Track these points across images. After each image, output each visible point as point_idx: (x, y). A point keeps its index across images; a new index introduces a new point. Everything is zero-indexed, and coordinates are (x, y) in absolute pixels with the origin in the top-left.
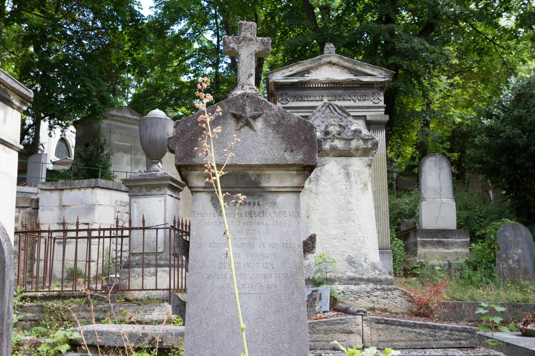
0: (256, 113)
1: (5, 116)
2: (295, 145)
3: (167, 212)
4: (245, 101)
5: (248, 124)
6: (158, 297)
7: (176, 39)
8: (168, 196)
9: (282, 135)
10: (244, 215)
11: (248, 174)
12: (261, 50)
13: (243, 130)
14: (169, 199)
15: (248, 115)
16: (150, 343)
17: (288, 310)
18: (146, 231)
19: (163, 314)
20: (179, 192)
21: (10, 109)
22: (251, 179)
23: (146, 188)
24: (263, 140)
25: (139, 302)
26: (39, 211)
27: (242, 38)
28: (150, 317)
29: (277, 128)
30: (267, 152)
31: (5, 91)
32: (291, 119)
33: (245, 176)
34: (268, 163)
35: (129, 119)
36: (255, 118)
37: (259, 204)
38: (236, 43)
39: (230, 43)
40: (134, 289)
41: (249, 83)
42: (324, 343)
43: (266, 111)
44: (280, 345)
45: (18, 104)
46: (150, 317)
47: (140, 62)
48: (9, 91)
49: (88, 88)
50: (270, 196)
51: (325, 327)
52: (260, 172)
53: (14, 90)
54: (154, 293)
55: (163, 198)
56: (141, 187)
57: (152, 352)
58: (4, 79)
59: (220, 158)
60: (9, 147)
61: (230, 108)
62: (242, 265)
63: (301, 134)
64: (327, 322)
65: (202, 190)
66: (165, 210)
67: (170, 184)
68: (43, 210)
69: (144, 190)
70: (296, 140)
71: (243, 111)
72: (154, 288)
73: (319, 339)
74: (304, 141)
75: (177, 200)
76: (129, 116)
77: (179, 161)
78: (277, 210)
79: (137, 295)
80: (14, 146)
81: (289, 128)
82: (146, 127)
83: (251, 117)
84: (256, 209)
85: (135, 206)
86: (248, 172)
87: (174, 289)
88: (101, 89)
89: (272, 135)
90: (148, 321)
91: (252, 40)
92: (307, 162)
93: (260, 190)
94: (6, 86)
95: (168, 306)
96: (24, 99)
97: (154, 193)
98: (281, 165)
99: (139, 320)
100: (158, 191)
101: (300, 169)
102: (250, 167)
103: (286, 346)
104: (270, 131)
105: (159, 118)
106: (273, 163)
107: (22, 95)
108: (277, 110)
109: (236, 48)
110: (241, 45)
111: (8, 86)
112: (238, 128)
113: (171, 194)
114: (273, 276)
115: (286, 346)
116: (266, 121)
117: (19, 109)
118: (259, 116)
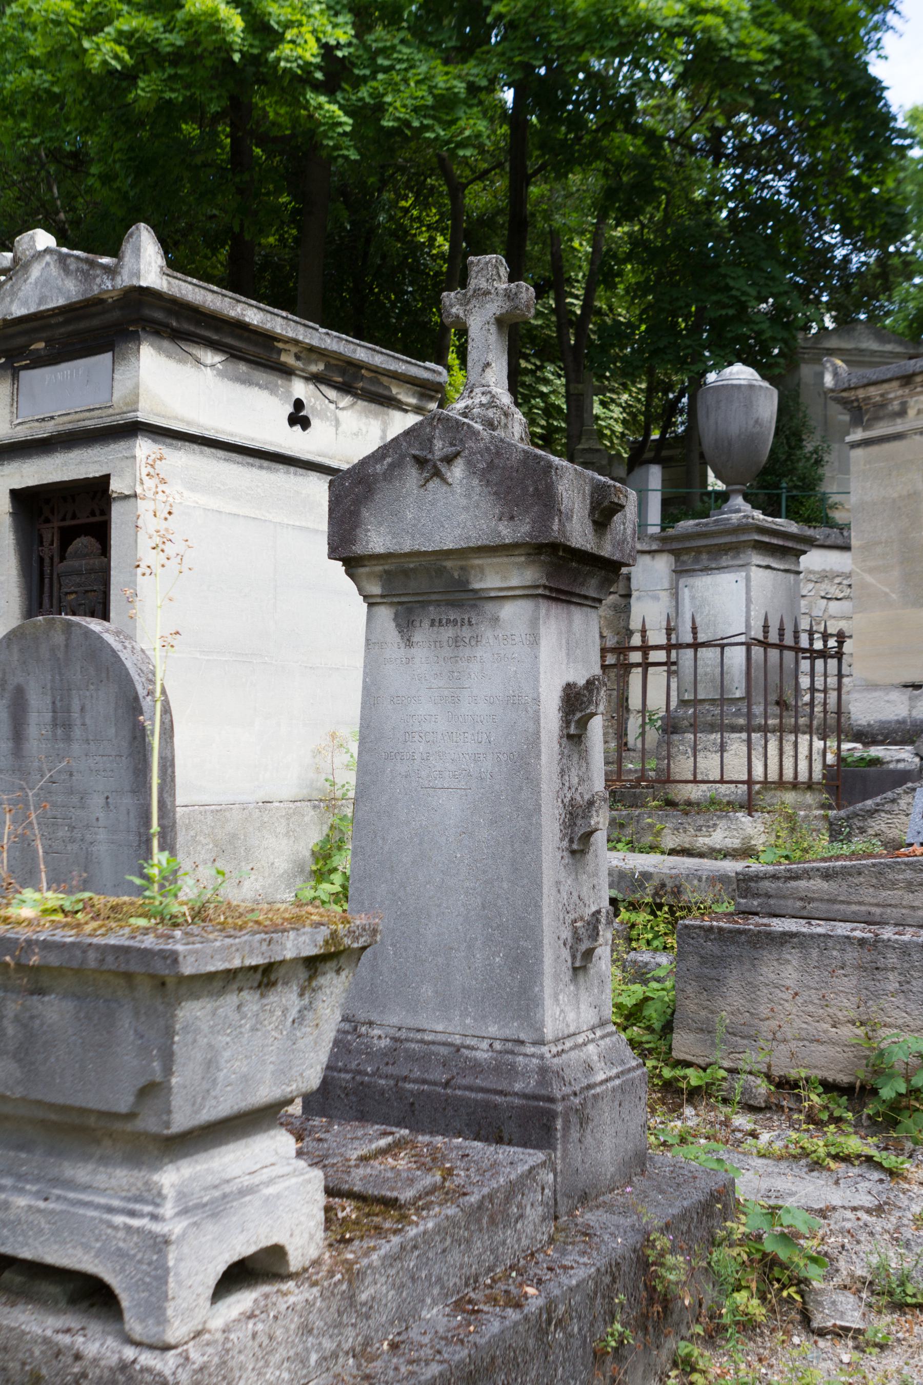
0: (450, 449)
2: (517, 506)
3: (752, 607)
4: (434, 428)
5: (437, 473)
6: (733, 797)
8: (754, 568)
10: (445, 644)
12: (504, 311)
13: (431, 485)
14: (758, 575)
15: (438, 454)
16: (656, 894)
17: (510, 820)
18: (702, 652)
19: (734, 837)
20: (798, 557)
22: (452, 576)
23: (709, 553)
24: (464, 502)
25: (690, 807)
26: (633, 601)
27: (471, 293)
28: (707, 840)
32: (511, 455)
33: (441, 571)
34: (471, 545)
35: (873, 353)
36: (449, 460)
37: (469, 622)
38: (461, 305)
39: (451, 306)
40: (684, 778)
42: (904, 911)
43: (470, 444)
44: (496, 883)
45: (413, 401)
46: (707, 840)
48: (385, 380)
49: (734, 293)
50: (489, 607)
51: (909, 875)
52: (463, 563)
53: (396, 376)
54: (723, 788)
55: (744, 574)
56: (698, 550)
57: (659, 913)
58: (366, 359)
61: (410, 445)
62: (440, 736)
63: (529, 482)
64: (912, 863)
65: (379, 600)
66: (749, 601)
67: (756, 541)
68: (638, 598)
69: (704, 556)
71: (431, 451)
72: (718, 778)
73: (893, 902)
74: (533, 495)
75: (792, 577)
76: (874, 346)
78: (499, 633)
79: (695, 792)
82: (707, 412)
83: (442, 460)
84: (466, 632)
85: (686, 594)
87: (765, 782)
89: (478, 490)
90: (705, 849)
91: (489, 293)
93: (471, 595)
95: (743, 819)
97: (724, 564)
99: (687, 846)
100: (733, 558)
101: (531, 551)
102: (448, 554)
103: (505, 885)
104: (476, 482)
105: (733, 386)
106: (480, 543)
109: (462, 315)
110: (471, 306)
112: (422, 483)
113: (764, 563)
114: (490, 757)
115: (505, 885)
116: (469, 463)
118: (457, 455)
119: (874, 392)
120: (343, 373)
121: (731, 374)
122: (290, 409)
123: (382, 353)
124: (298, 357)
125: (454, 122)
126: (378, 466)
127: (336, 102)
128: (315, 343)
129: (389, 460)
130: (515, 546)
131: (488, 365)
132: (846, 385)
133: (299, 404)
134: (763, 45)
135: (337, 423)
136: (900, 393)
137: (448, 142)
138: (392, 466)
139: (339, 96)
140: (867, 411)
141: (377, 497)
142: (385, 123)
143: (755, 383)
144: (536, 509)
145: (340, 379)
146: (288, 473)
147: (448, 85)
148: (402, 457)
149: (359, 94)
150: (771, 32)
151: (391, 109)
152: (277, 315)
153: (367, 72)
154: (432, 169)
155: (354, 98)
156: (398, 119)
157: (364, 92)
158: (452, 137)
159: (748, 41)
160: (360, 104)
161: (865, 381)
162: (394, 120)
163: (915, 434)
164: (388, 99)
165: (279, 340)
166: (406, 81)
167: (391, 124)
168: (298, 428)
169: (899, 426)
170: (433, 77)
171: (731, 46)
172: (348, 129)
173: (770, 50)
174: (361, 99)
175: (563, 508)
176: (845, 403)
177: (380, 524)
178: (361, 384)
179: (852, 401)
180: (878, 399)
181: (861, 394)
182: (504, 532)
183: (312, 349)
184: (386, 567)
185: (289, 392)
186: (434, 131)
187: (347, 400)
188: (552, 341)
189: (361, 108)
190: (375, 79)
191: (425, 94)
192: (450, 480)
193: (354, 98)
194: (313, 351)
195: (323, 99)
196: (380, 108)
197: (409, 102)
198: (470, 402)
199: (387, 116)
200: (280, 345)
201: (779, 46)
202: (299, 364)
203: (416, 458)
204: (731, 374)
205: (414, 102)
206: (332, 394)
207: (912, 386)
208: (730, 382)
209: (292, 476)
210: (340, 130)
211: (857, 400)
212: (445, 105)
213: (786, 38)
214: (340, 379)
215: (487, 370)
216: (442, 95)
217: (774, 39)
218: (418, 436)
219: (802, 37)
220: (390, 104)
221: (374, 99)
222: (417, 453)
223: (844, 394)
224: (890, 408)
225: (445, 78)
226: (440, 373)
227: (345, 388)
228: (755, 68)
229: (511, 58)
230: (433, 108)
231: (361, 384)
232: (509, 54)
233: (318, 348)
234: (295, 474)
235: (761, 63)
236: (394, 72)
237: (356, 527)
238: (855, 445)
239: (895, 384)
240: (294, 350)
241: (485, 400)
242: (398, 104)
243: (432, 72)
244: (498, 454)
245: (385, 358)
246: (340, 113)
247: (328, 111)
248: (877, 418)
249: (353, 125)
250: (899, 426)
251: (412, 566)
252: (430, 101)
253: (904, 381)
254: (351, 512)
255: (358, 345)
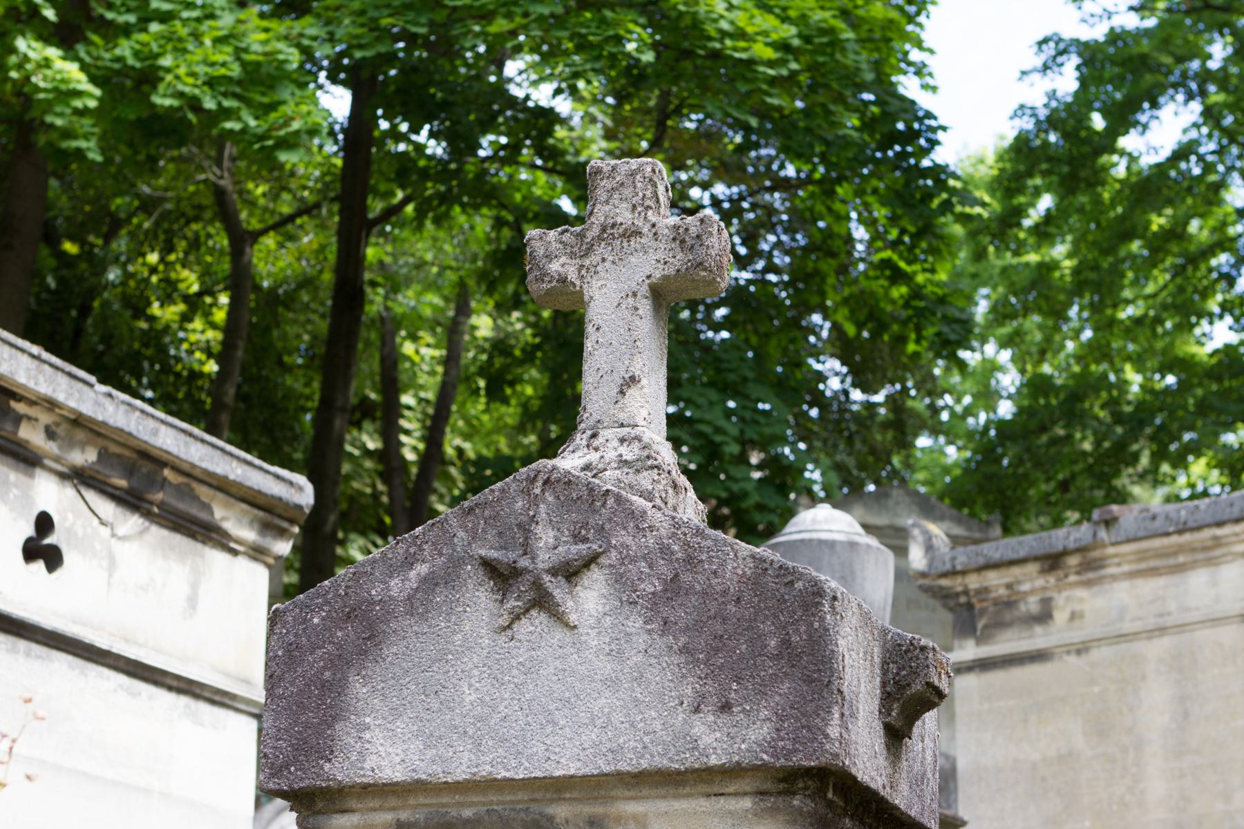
0: (574, 549)
1: (194, 587)
2: (738, 679)
4: (535, 501)
5: (542, 601)
7: (1152, 187)
9: (683, 640)
11: (551, 819)
12: (671, 271)
13: (524, 628)
15: (545, 559)
21: (216, 558)
24: (606, 667)
27: (595, 231)
29: (666, 611)
30: (617, 717)
31: (185, 492)
32: (723, 564)
34: (624, 767)
36: (571, 572)
38: (572, 255)
39: (549, 257)
41: (622, 416)
43: (622, 537)
45: (249, 534)
47: (942, 300)
48: (203, 492)
52: (598, 810)
53: (223, 486)
58: (174, 450)
59: (430, 753)
60: (213, 702)
61: (474, 536)
63: (767, 627)
70: (741, 658)
71: (527, 549)
74: (778, 657)
77: (273, 775)
80: (234, 697)
81: (713, 607)
83: (554, 572)
86: (550, 810)
88: (768, 431)
89: (641, 640)
91: (638, 233)
92: (789, 754)
94: (188, 475)
96: (270, 513)
98: (678, 772)
101: (768, 786)
104: (635, 623)
106: (644, 764)
107: (260, 501)
108: (665, 529)
109: (572, 275)
110: (594, 258)
111: (197, 473)
112: (503, 621)
116: (618, 579)
117: (257, 553)
118: (591, 561)
119: (995, 580)
120: (129, 470)
121: (814, 521)
122: (29, 531)
123: (203, 441)
124: (50, 434)
125: (273, 106)
126: (395, 583)
127: (76, 58)
128: (87, 409)
129: (422, 569)
130: (731, 772)
131: (633, 380)
132: (948, 566)
133: (44, 523)
134: (774, 37)
135: (112, 563)
136: (1040, 582)
137: (262, 138)
138: (429, 583)
139: (81, 49)
140: (983, 612)
141: (389, 651)
142: (157, 100)
143: (857, 539)
144: (785, 687)
145: (123, 483)
146: (14, 651)
147: (268, 48)
148: (456, 563)
149: (118, 52)
150: (785, 19)
151: (169, 78)
152: (23, 350)
153: (131, 18)
154: (200, 208)
155: (107, 56)
156: (181, 95)
157: (125, 49)
158: (269, 130)
159: (750, 30)
160: (117, 66)
161: (981, 561)
162: (173, 96)
163: (1068, 652)
164: (166, 61)
165: (19, 398)
166: (197, 36)
167: (168, 102)
168: (40, 566)
169: (1038, 639)
170: (244, 35)
171: (724, 34)
172: (92, 104)
173: (783, 46)
174: (120, 59)
175: (845, 689)
176: (945, 597)
177: (396, 713)
178: (159, 496)
179: (957, 595)
180: (1002, 592)
181: (973, 582)
182: (707, 740)
183: (78, 422)
184: (404, 816)
185: (27, 498)
186: (239, 119)
187: (132, 522)
188: (363, 501)
189: (117, 73)
190: (145, 30)
191: (228, 59)
192: (573, 618)
193: (107, 56)
194: (80, 426)
195: (53, 53)
196: (149, 77)
197: (201, 69)
198: (593, 457)
199: (161, 88)
200: (20, 408)
201: (796, 42)
202: (52, 447)
203: (490, 567)
204: (814, 521)
205: (209, 70)
206: (107, 508)
207: (1061, 573)
208: (815, 536)
209: (21, 658)
210: (78, 103)
211: (966, 592)
212: (260, 81)
213: (806, 32)
214: (123, 483)
215: (632, 392)
216: (258, 64)
217: (788, 31)
218: (496, 517)
219: (831, 31)
220: (168, 70)
221: (142, 60)
222: (493, 554)
223: (944, 582)
224: (1023, 607)
225: (263, 36)
226: (301, 489)
227: (131, 501)
228: (761, 69)
229: (376, 20)
230: (239, 83)
231: (159, 496)
232: (372, 13)
233: (92, 420)
234: (28, 655)
235: (771, 64)
236: (178, 23)
237: (335, 718)
238: (964, 668)
239: (1032, 568)
240: (45, 418)
241: (629, 453)
242: (182, 71)
243: (242, 28)
244: (690, 561)
245: (209, 450)
246: (82, 77)
247: (60, 72)
248: (999, 625)
249: (100, 99)
250: (1038, 639)
251: (468, 813)
252: (235, 71)
253: (1047, 564)
254: (324, 686)
255: (163, 422)
